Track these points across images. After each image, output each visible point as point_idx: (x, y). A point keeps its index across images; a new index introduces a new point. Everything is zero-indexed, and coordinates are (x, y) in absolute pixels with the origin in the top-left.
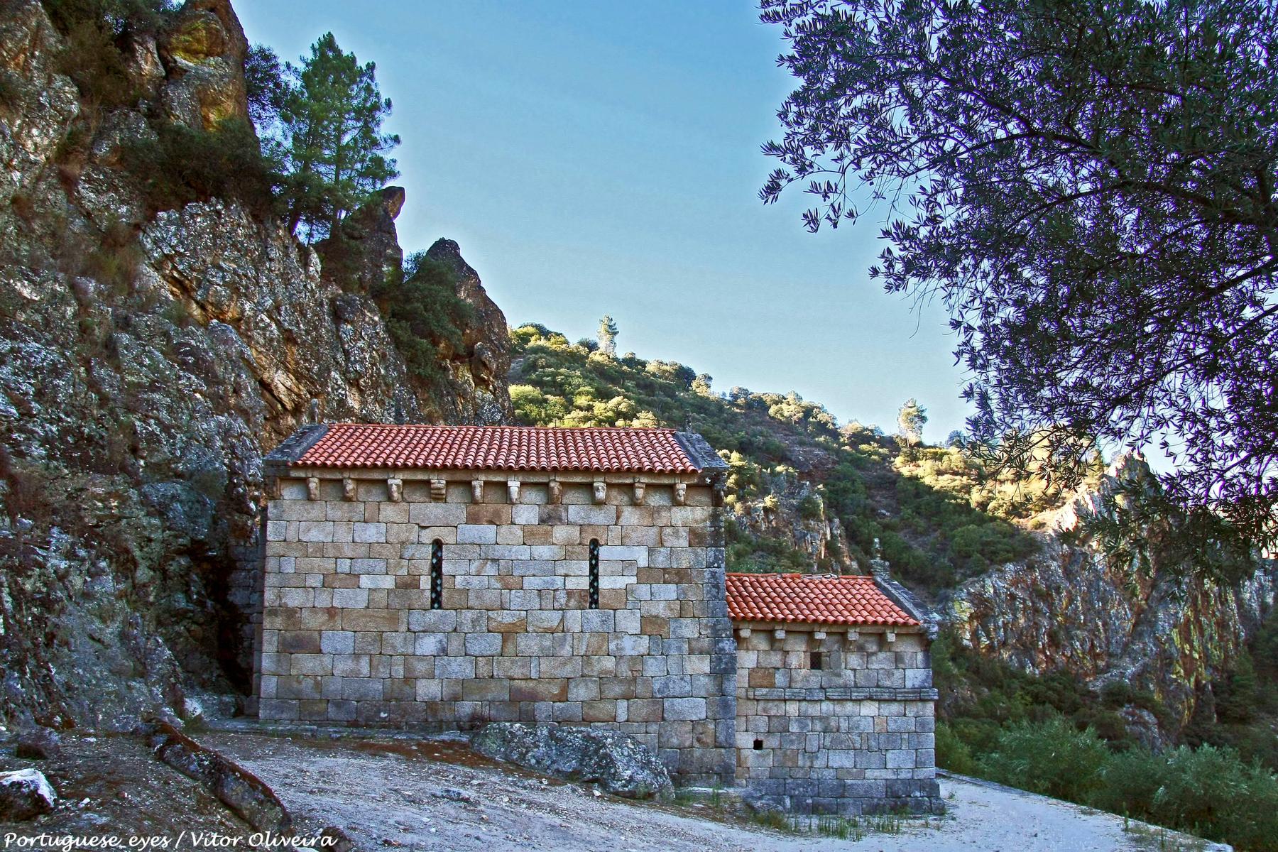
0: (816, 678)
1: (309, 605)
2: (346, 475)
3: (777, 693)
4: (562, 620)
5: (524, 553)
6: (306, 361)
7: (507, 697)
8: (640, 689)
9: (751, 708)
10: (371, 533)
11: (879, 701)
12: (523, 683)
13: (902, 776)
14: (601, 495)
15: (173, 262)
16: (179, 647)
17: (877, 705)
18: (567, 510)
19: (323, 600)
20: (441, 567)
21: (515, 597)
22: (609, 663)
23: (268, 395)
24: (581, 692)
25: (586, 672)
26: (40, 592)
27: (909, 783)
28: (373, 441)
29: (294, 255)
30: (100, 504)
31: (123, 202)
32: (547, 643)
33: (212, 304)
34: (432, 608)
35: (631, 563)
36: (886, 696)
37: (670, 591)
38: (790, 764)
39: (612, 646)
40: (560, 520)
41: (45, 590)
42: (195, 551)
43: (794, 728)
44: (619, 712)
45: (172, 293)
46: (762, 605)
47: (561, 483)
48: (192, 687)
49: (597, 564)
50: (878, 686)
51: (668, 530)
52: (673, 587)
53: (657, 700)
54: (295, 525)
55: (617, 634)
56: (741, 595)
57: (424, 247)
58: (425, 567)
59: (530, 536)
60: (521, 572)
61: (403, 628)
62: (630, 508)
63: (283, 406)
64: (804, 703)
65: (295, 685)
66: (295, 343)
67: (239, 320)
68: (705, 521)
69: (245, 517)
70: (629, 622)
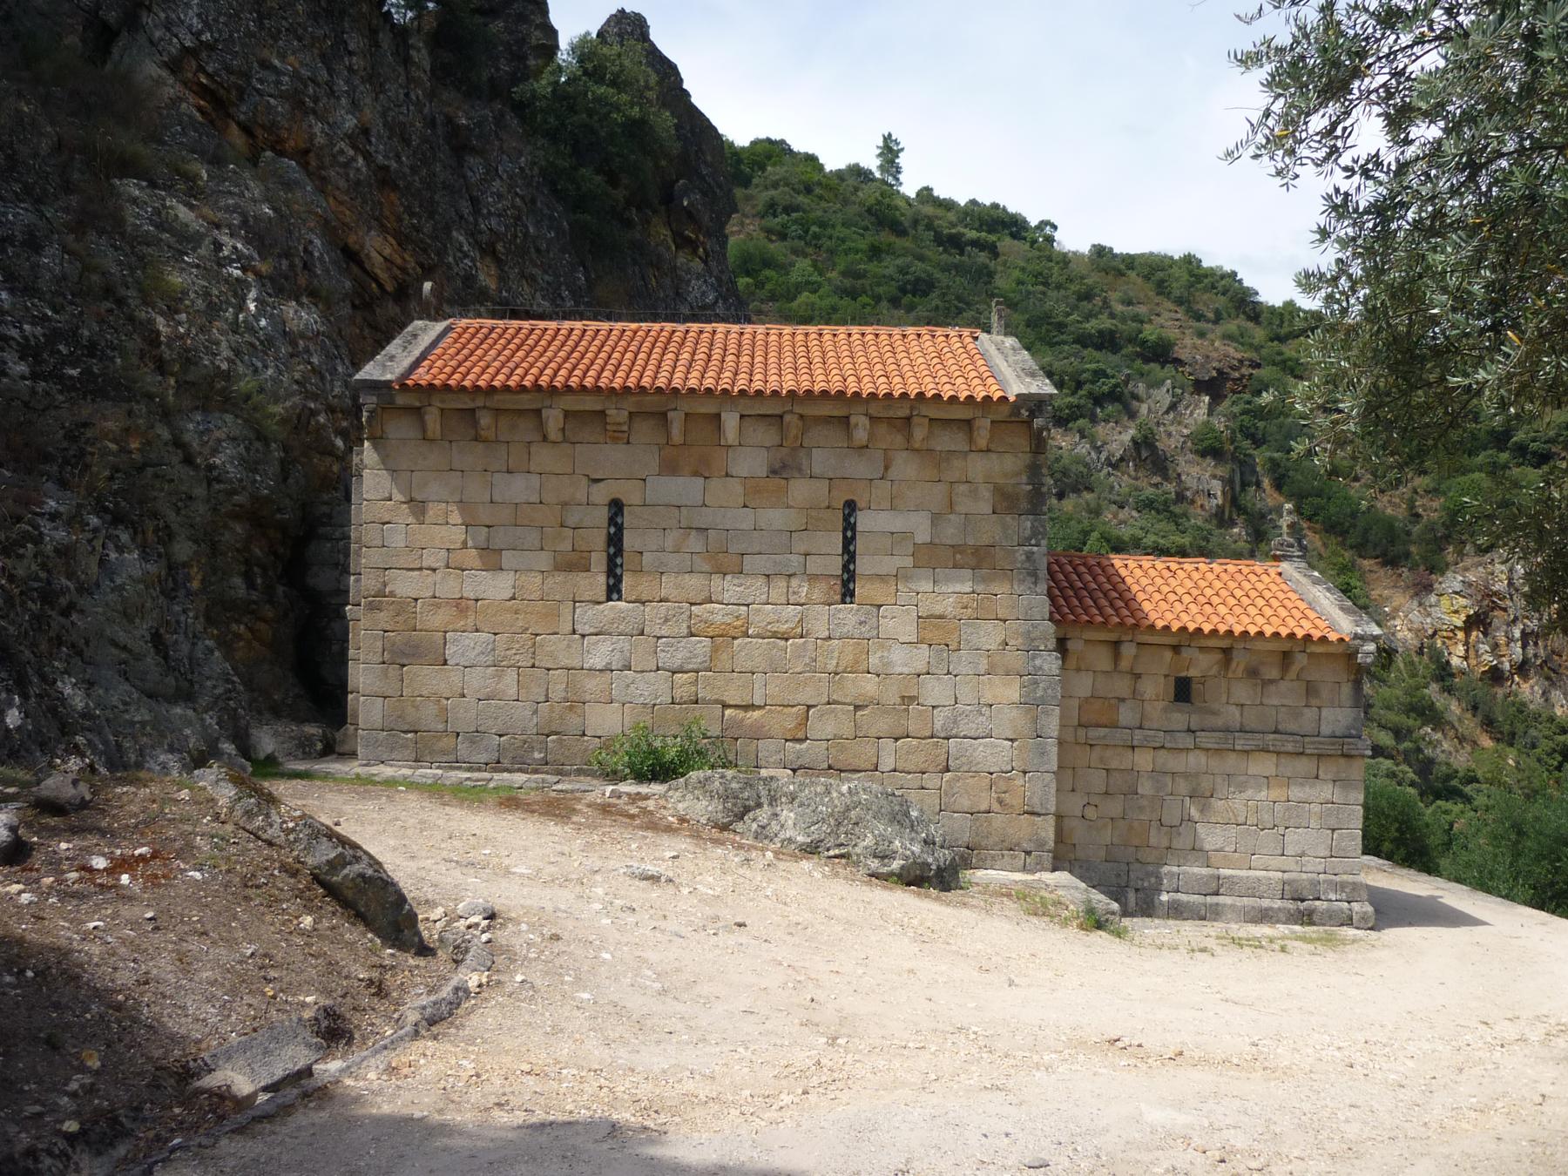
0: (1179, 719)
2: (480, 402)
5: (745, 519)
6: (412, 215)
11: (1278, 753)
12: (741, 714)
14: (861, 435)
15: (197, 58)
16: (239, 655)
17: (1274, 758)
18: (810, 455)
20: (621, 540)
22: (869, 686)
23: (355, 269)
24: (824, 726)
26: (37, 579)
28: (519, 348)
29: (385, 39)
30: (113, 446)
33: (263, 127)
34: (609, 599)
35: (906, 535)
36: (1290, 747)
38: (1136, 842)
39: (874, 660)
40: (800, 470)
41: (43, 575)
42: (257, 517)
43: (1145, 788)
45: (199, 109)
46: (1104, 602)
48: (260, 713)
49: (854, 538)
51: (963, 488)
55: (886, 641)
56: (1072, 587)
57: (592, 25)
59: (753, 495)
60: (741, 548)
62: (905, 454)
63: (380, 286)
64: (1162, 752)
66: (395, 188)
67: (306, 152)
68: (1019, 474)
69: (329, 460)
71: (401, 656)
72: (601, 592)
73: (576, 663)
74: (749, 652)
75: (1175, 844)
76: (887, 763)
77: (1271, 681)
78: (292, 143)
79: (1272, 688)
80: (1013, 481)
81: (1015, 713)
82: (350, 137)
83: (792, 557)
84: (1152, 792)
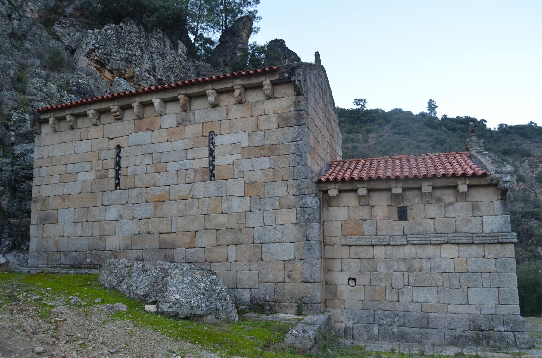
0: (399, 226)
1: (53, 194)
3: (365, 240)
4: (191, 190)
5: (167, 147)
7: (157, 246)
8: (245, 238)
9: (344, 252)
10: (84, 147)
13: (485, 311)
19: (59, 190)
21: (162, 179)
22: (222, 219)
24: (203, 240)
25: (207, 226)
27: (491, 317)
31: (77, 31)
32: (181, 207)
33: (115, 70)
34: (116, 189)
36: (464, 240)
37: (265, 162)
38: (379, 298)
39: (224, 206)
40: (190, 121)
43: (382, 268)
44: (230, 254)
45: (95, 67)
47: (186, 95)
50: (456, 232)
51: (263, 118)
52: (267, 159)
53: (258, 244)
54: (47, 147)
58: (111, 164)
61: (99, 204)
64: (389, 248)
65: (45, 243)
67: (133, 77)
68: (289, 107)
70: (236, 187)
71: (45, 220)
72: (113, 186)
73: (103, 219)
74: (171, 208)
75: (401, 299)
76: (232, 258)
77: (450, 204)
78: (127, 75)
79: (451, 208)
80: (287, 110)
81: (294, 228)
82: (147, 71)
83: (187, 161)
84: (385, 270)
